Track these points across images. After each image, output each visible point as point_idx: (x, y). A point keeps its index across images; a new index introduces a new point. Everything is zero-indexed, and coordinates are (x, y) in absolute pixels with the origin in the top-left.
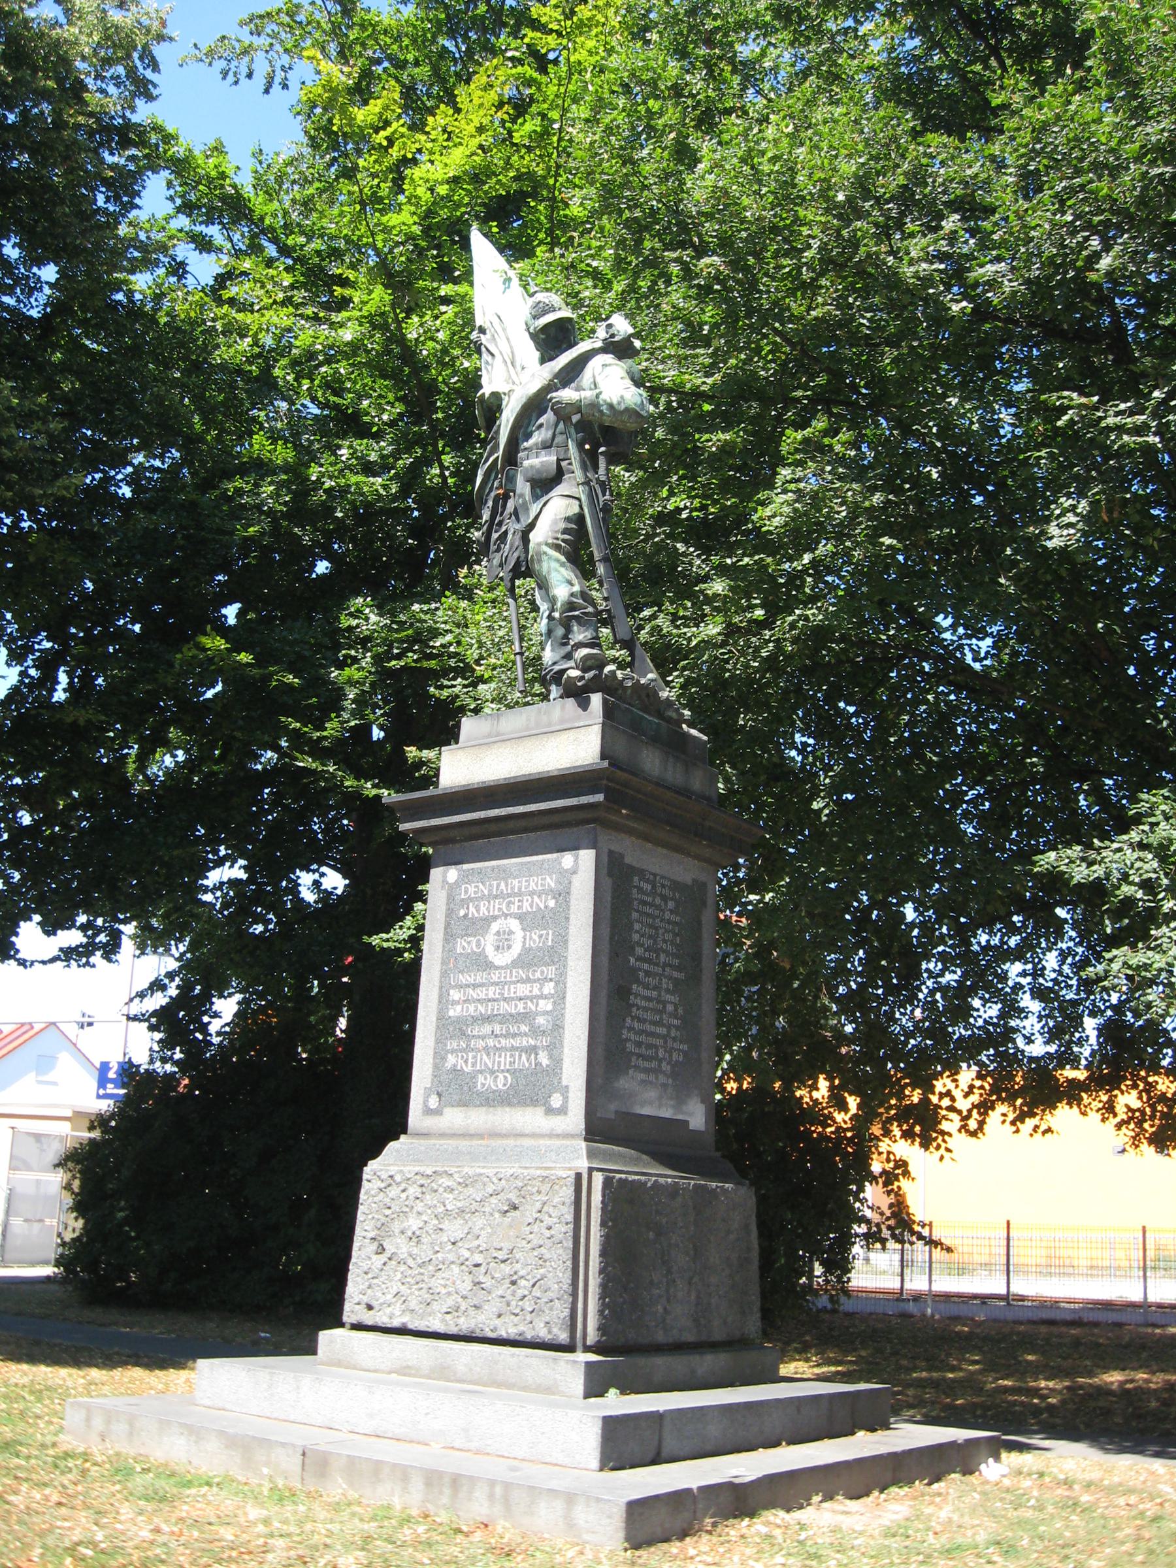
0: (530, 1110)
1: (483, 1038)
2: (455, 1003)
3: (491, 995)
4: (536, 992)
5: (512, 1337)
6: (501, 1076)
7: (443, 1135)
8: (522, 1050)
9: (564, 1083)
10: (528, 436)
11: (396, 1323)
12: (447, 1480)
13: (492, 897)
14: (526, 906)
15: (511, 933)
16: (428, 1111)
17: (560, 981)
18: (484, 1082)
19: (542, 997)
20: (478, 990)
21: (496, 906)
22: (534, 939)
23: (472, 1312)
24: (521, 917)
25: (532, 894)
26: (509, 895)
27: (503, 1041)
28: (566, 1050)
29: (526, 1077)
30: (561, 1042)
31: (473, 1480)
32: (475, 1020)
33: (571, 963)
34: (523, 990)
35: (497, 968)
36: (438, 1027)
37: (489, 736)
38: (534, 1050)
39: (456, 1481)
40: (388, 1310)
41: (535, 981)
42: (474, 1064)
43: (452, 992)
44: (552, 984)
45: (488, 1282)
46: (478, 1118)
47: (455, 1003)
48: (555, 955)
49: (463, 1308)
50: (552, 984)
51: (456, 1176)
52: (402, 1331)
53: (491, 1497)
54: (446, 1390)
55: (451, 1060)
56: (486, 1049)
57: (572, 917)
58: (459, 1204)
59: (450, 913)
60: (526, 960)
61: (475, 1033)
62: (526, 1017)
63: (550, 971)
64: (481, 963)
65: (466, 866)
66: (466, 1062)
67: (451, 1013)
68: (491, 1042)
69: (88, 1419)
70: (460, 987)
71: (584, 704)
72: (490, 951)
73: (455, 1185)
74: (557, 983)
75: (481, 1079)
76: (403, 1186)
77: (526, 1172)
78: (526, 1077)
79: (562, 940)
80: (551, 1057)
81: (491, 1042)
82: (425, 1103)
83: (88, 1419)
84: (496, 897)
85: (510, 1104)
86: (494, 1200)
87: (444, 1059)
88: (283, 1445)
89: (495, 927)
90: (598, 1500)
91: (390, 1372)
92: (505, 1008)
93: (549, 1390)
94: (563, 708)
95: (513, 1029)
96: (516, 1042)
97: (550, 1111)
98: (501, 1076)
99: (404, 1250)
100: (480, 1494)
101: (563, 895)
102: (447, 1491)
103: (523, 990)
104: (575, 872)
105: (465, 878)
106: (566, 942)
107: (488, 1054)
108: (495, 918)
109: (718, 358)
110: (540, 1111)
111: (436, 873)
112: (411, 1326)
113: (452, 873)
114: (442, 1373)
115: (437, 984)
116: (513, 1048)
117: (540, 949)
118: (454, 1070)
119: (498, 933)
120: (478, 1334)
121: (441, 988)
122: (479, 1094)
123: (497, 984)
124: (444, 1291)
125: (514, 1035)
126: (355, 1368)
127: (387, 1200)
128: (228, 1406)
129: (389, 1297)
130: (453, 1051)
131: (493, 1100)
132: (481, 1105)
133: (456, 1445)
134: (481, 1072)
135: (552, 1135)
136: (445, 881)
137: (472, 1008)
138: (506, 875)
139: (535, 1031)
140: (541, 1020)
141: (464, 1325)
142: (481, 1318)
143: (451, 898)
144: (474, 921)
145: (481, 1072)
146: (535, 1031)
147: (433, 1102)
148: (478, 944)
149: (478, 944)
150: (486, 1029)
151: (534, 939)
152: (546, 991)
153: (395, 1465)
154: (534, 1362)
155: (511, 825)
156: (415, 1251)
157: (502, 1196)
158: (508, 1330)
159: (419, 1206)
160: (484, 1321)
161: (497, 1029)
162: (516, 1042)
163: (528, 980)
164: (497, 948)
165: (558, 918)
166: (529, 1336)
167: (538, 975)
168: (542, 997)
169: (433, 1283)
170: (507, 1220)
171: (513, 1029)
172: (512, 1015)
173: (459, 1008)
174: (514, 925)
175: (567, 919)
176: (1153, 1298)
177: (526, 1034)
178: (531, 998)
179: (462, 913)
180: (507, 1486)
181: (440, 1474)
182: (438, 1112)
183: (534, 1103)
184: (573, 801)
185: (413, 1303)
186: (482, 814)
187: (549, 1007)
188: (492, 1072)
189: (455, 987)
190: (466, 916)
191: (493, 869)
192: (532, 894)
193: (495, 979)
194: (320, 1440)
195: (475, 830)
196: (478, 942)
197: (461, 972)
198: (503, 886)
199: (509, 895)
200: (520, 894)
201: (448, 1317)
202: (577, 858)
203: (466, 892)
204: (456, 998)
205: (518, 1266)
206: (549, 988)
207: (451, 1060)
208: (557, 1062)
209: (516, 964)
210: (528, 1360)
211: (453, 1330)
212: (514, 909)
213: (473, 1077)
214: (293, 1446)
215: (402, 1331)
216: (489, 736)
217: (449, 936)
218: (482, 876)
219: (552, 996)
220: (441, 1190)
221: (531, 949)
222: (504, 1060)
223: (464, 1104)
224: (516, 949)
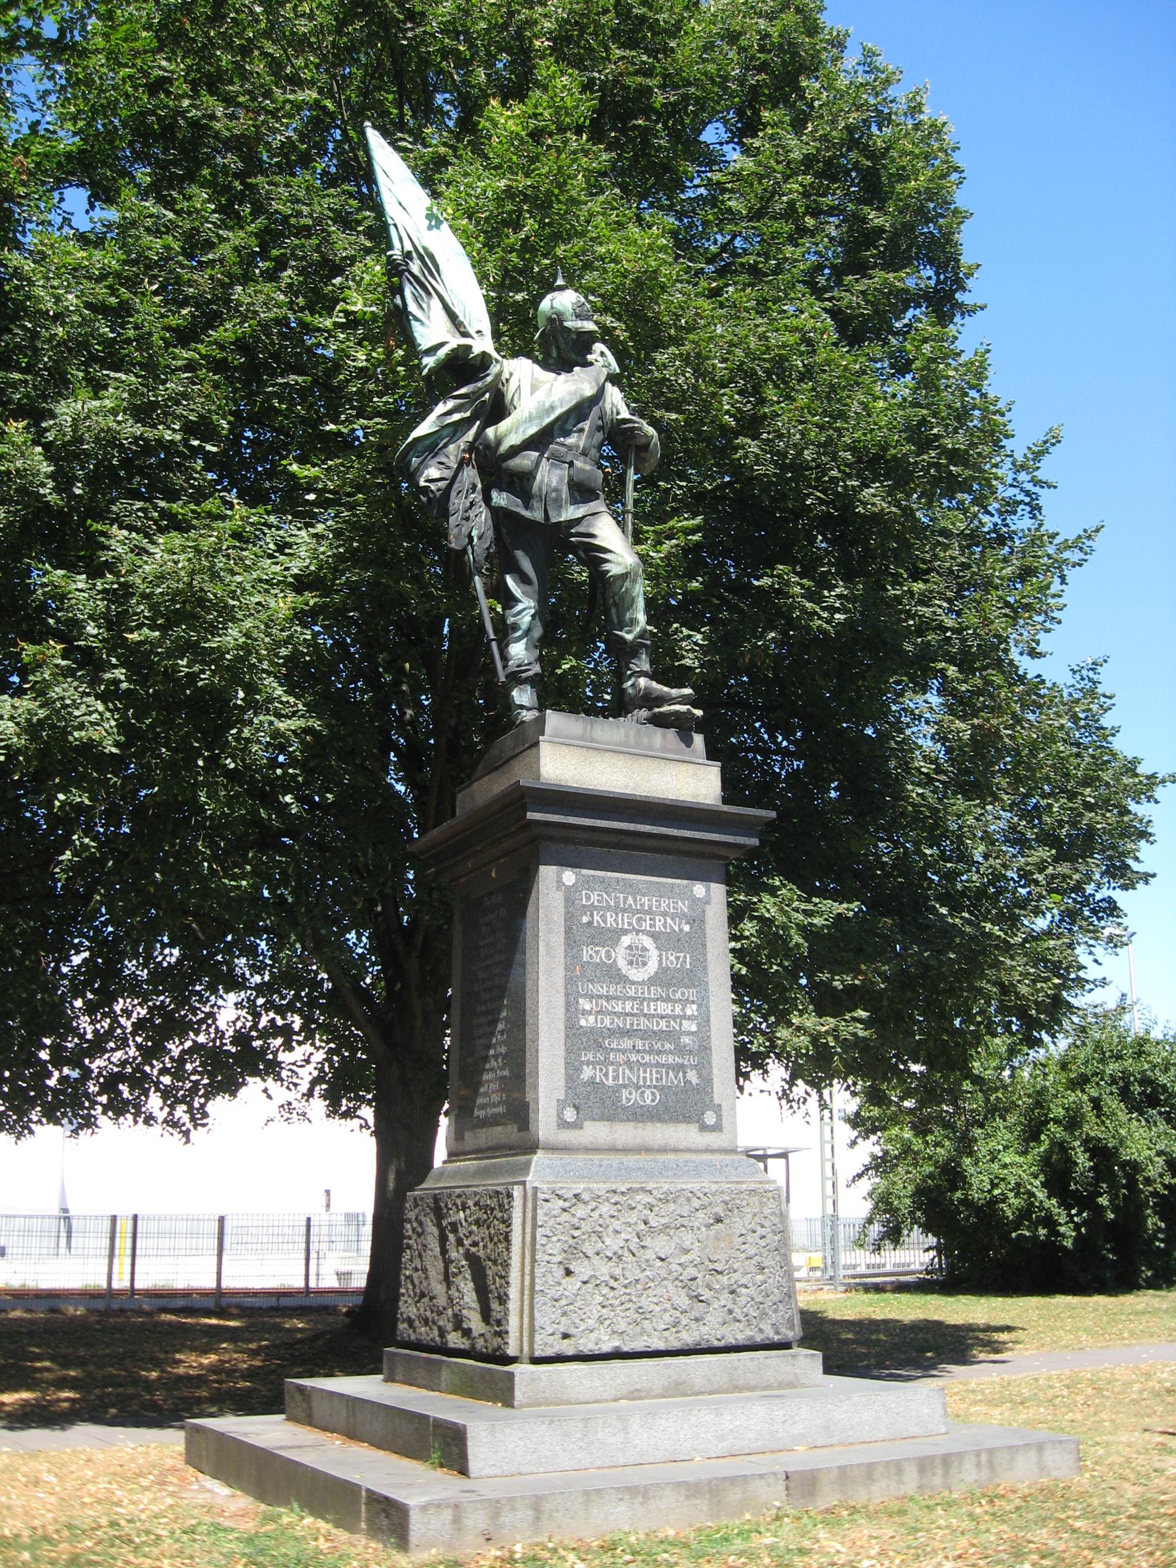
0: (682, 1126)
1: (624, 1052)
2: (585, 1013)
3: (628, 1009)
4: (678, 1011)
5: (741, 1343)
6: (648, 1092)
7: (588, 1150)
8: (669, 1067)
9: (717, 1101)
10: (567, 434)
11: (606, 1348)
12: (938, 1461)
13: (617, 910)
14: (659, 925)
15: (645, 949)
16: (563, 1125)
17: (703, 1002)
18: (629, 1097)
19: (684, 1017)
20: (613, 1002)
21: (624, 921)
22: (671, 959)
23: (694, 1325)
24: (655, 936)
25: (665, 914)
26: (638, 912)
27: (647, 1058)
28: (715, 1071)
29: (675, 1094)
30: (710, 1063)
31: (960, 1455)
32: (612, 1033)
33: (712, 987)
34: (663, 1008)
35: (633, 983)
36: (567, 1036)
37: (581, 738)
38: (681, 1068)
39: (947, 1461)
40: (593, 1336)
41: (676, 1001)
42: (616, 1078)
43: (581, 1001)
44: (694, 1007)
45: (706, 1295)
46: (626, 1133)
47: (585, 1013)
48: (694, 978)
49: (684, 1322)
50: (694, 1007)
51: (655, 1192)
52: (617, 1355)
53: (978, 1465)
54: (748, 1399)
55: (587, 1073)
56: (628, 1063)
57: (709, 945)
58: (663, 1221)
59: (569, 918)
60: (663, 978)
61: (614, 1046)
62: (668, 1035)
63: (691, 993)
64: (613, 974)
65: (584, 871)
66: (606, 1075)
67: (583, 1023)
68: (634, 1057)
69: (457, 1520)
70: (591, 997)
71: (688, 742)
72: (622, 964)
73: (655, 1202)
74: (700, 1006)
75: (625, 1093)
76: (593, 1204)
77: (732, 1186)
78: (675, 1094)
79: (701, 963)
80: (700, 1076)
81: (634, 1057)
82: (560, 1115)
83: (457, 1520)
84: (624, 910)
85: (660, 1120)
86: (700, 1214)
87: (579, 1070)
88: (761, 1476)
89: (626, 940)
90: (1060, 1442)
91: (616, 1400)
92: (644, 1023)
93: (791, 1385)
94: (664, 736)
95: (658, 1046)
96: (663, 1059)
97: (704, 1128)
98: (648, 1092)
99: (605, 1270)
100: (969, 1464)
101: (697, 921)
102: (939, 1472)
103: (663, 1008)
104: (708, 903)
105: (588, 884)
106: (705, 968)
107: (631, 1069)
108: (625, 932)
109: (125, 262)
110: (693, 1128)
111: (547, 874)
112: (626, 1349)
113: (569, 876)
114: (677, 1389)
115: (562, 990)
116: (658, 1065)
117: (677, 970)
118: (592, 1081)
119: (630, 947)
120: (704, 1345)
121: (567, 995)
122: (624, 1109)
123: (634, 999)
124: (658, 1308)
125: (659, 1052)
126: (569, 1403)
127: (575, 1221)
128: (523, 1469)
129: (591, 1322)
130: (588, 1063)
131: (640, 1115)
132: (628, 1120)
133: (818, 1443)
134: (625, 1086)
135: (708, 1150)
136: (560, 881)
137: (607, 1021)
138: (635, 891)
139: (681, 1050)
140: (686, 1040)
141: (688, 1338)
142: (704, 1330)
143: (569, 901)
144: (601, 931)
145: (625, 1086)
146: (681, 1050)
147: (570, 1115)
148: (608, 956)
149: (608, 956)
150: (627, 1043)
151: (671, 959)
152: (689, 1012)
153: (888, 1462)
154: (774, 1361)
155: (650, 843)
156: (617, 1272)
157: (709, 1210)
158: (738, 1334)
159: (616, 1224)
160: (713, 1330)
161: (639, 1044)
162: (663, 1059)
163: (668, 1000)
164: (631, 963)
165: (695, 942)
166: (759, 1338)
167: (678, 995)
168: (684, 1017)
169: (644, 1301)
170: (712, 1233)
171: (658, 1046)
172: (654, 1032)
173: (591, 1019)
174: (647, 942)
175: (704, 946)
176: (227, 1283)
177: (671, 1052)
178: (674, 1018)
179: (585, 919)
180: (991, 1452)
181: (932, 1458)
182: (577, 1125)
183: (687, 1120)
184: (730, 839)
185: (622, 1326)
186: (647, 828)
187: (694, 1028)
188: (638, 1087)
189: (585, 996)
190: (590, 923)
191: (617, 880)
192: (665, 914)
193: (632, 993)
194: (801, 1459)
195: (596, 837)
196: (608, 952)
197: (592, 982)
198: (630, 900)
199: (638, 912)
200: (650, 912)
201: (666, 1334)
202: (708, 890)
203: (588, 898)
204: (587, 1007)
205: (736, 1276)
206: (691, 1010)
207: (587, 1073)
208: (707, 1081)
209: (652, 981)
210: (768, 1361)
211: (676, 1345)
212: (646, 925)
213: (617, 1089)
214: (774, 1474)
215: (617, 1355)
216: (581, 738)
217: (572, 943)
218: (607, 887)
219: (696, 1018)
220: (640, 1207)
221: (668, 969)
222: (650, 1076)
223: (603, 1118)
224: (652, 967)
